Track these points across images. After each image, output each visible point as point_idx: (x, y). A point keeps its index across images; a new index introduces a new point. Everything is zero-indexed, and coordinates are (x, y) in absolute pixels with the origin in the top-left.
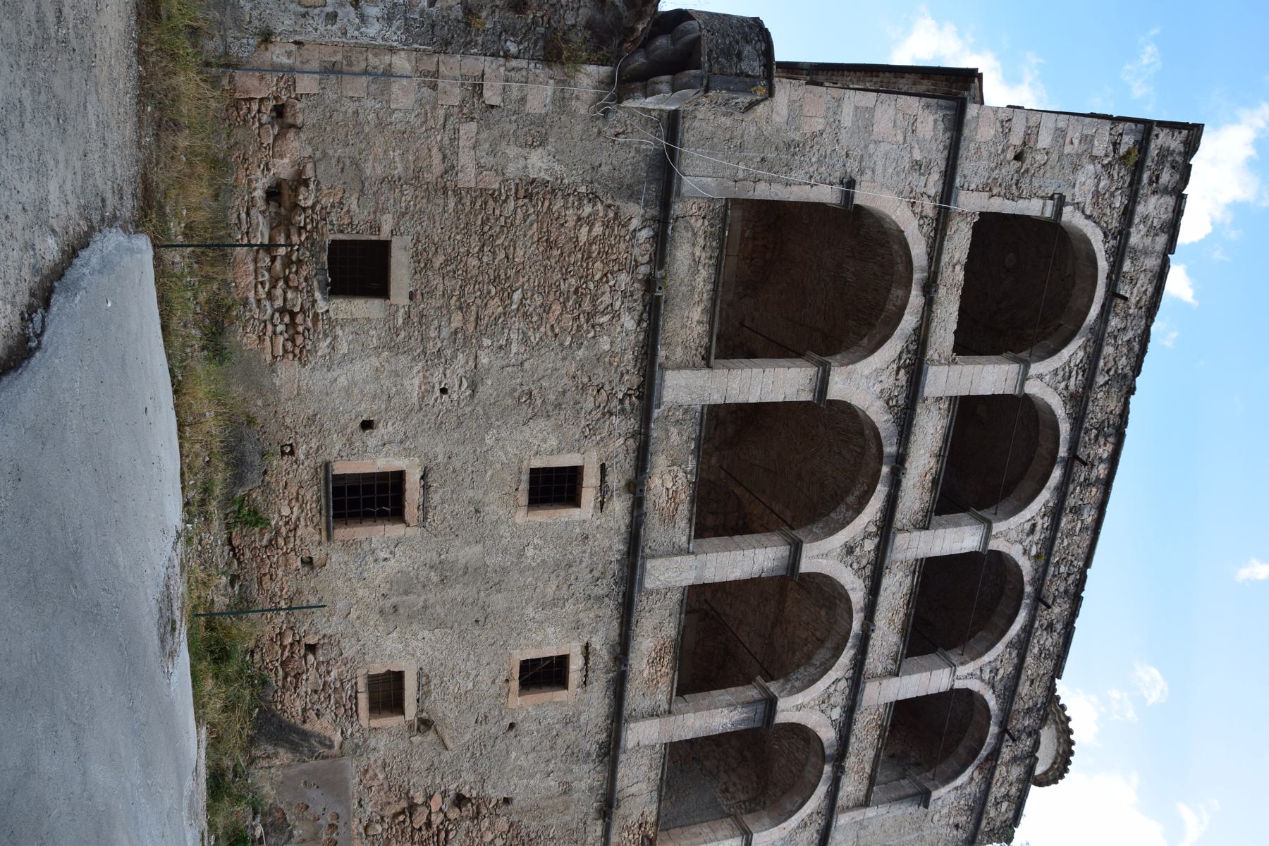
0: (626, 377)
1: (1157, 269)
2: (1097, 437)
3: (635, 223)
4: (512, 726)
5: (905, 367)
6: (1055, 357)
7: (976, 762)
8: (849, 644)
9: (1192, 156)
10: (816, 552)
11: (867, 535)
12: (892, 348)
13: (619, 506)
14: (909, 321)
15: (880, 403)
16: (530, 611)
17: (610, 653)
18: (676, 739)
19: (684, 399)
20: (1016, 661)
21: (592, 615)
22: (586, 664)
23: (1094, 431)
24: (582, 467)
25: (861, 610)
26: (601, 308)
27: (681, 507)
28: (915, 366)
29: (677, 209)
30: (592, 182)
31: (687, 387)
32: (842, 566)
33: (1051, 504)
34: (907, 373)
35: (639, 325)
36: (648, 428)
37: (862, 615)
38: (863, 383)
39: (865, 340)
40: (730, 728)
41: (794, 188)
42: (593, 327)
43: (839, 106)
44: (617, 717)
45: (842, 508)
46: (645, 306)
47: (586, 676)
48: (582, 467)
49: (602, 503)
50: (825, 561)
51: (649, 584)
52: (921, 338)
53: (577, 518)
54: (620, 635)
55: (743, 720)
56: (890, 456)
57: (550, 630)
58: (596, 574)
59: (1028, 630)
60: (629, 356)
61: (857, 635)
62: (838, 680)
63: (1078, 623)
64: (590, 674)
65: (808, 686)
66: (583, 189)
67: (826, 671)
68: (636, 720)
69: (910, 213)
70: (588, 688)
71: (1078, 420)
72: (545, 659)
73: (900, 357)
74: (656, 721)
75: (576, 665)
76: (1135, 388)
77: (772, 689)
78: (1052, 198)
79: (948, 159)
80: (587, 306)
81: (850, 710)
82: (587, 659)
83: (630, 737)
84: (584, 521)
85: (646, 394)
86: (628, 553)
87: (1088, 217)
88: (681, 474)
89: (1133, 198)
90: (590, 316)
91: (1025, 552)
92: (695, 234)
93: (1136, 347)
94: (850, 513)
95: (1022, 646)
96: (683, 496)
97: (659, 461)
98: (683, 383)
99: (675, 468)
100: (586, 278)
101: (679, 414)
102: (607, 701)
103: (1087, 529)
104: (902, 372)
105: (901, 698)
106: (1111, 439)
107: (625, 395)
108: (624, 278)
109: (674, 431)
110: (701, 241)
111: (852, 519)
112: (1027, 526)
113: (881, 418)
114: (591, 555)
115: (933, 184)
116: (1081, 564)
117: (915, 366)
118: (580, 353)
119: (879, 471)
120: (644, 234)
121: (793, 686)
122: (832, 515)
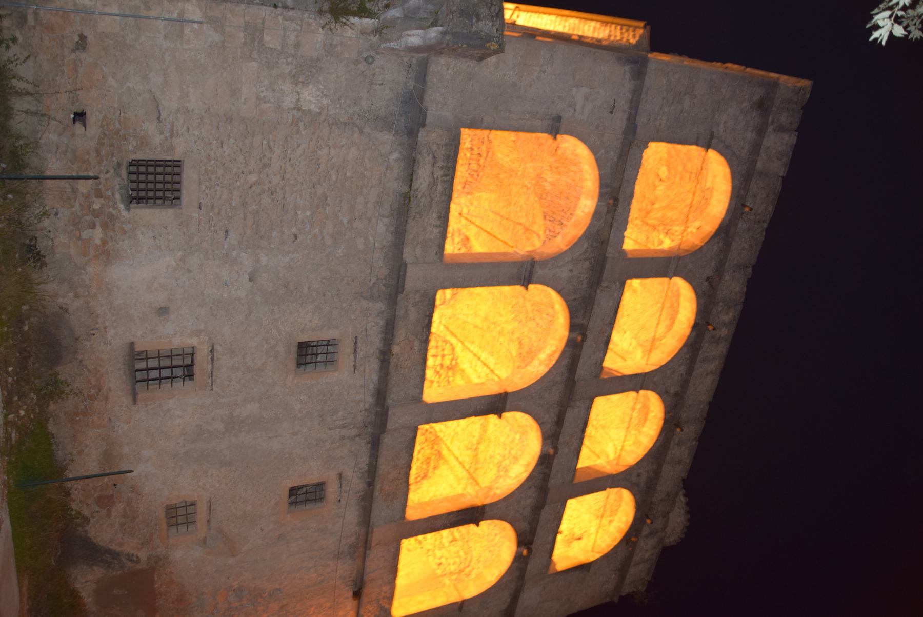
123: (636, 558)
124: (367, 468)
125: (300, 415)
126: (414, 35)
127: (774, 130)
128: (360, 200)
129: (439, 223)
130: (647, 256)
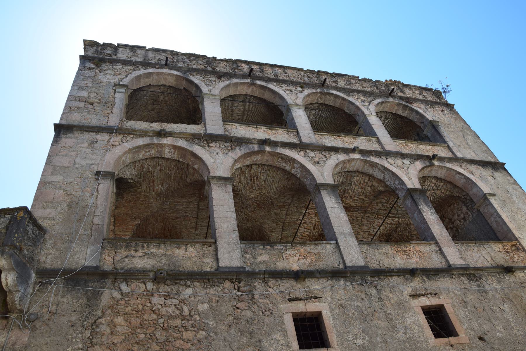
0: (226, 291)
1: (154, 52)
2: (238, 69)
3: (116, 294)
4: (481, 338)
5: (208, 143)
6: (199, 85)
7: (409, 105)
8: (368, 159)
9: (99, 43)
10: (321, 178)
11: (306, 155)
12: (198, 150)
13: (315, 285)
14: (182, 143)
15: (230, 154)
16: (400, 336)
17: (412, 281)
18: (450, 238)
19: (237, 254)
20: (356, 93)
21: (391, 295)
22: (424, 295)
23: (236, 71)
24: (293, 313)
25: (348, 155)
26: (177, 312)
27: (309, 250)
28: (209, 139)
29: (108, 267)
30: (83, 326)
31: (229, 253)
32: (326, 165)
33: (275, 84)
34: (211, 142)
35: (189, 286)
36: (260, 273)
37: (350, 155)
38: (219, 162)
39: (196, 167)
40: (433, 210)
41: (99, 203)
42: (192, 316)
43: (49, 183)
44: (449, 270)
45: (294, 171)
46: (176, 283)
47: (431, 294)
48: (293, 313)
49: (316, 298)
50: (325, 173)
51: (362, 263)
52: (193, 138)
53: (329, 313)
54: (398, 276)
55: (426, 204)
56: (259, 147)
57: (409, 321)
58: (364, 296)
59: (340, 89)
60: (212, 291)
61: (362, 156)
62: (388, 162)
63: (331, 71)
64: (429, 292)
65: (397, 176)
66: (88, 333)
67: (386, 169)
68: (447, 261)
69: (118, 147)
70: (438, 291)
71: (230, 76)
72: (429, 323)
73: (203, 146)
74: (444, 249)
75: (427, 301)
76: (213, 57)
77: (403, 194)
78: (115, 90)
79: (89, 131)
80: (178, 322)
81: (403, 156)
82: (420, 295)
83: (459, 263)
84: (330, 307)
85: (237, 276)
86: (345, 277)
87: (126, 76)
88: (288, 252)
89: (117, 61)
90: (183, 318)
91: (301, 92)
92: (126, 257)
93: (192, 58)
94: (295, 165)
95: (349, 91)
96: (302, 250)
97: (281, 265)
98: (227, 256)
99: (284, 256)
100: (155, 323)
101: (248, 256)
102: (442, 279)
103: (284, 71)
104: (211, 145)
105: (389, 136)
106: (239, 65)
107: (238, 290)
108: (157, 300)
109: (260, 259)
110: (132, 252)
111: (299, 163)
112: (288, 92)
113: (238, 152)
114: (351, 300)
115: (103, 137)
116: (302, 73)
117: (209, 139)
118: (211, 323)
119: (269, 152)
120: (124, 287)
121: (399, 184)
122: (298, 176)
123: (420, 97)
124: (401, 277)
125: (367, 338)
126: (6, 280)
127: (116, 55)
128: (163, 311)
129: (183, 233)
130: (203, 114)
